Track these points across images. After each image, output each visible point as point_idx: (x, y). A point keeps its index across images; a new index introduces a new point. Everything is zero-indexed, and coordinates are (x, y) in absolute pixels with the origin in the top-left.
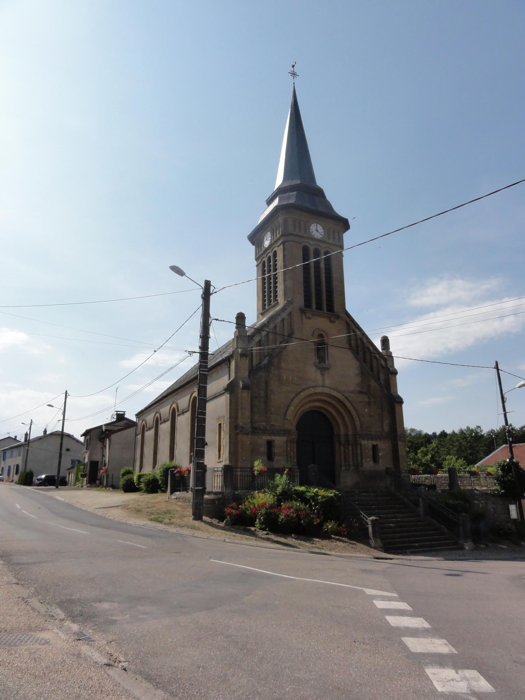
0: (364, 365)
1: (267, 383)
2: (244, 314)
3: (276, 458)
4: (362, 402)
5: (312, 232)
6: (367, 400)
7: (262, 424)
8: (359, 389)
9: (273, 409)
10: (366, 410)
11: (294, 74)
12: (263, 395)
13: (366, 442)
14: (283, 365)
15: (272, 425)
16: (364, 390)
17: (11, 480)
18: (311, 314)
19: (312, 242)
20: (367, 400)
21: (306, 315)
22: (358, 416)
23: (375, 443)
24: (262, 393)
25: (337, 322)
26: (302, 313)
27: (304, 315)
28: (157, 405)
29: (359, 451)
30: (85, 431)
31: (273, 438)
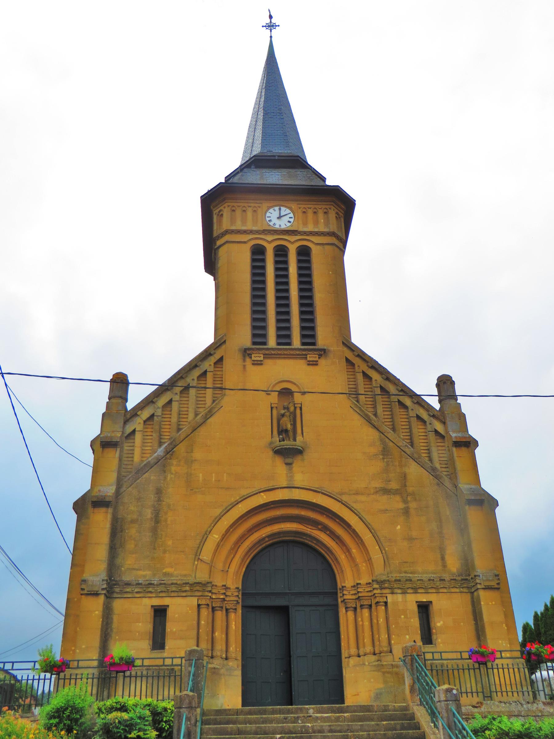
0: (391, 434)
1: (159, 492)
2: (126, 376)
3: (169, 643)
4: (385, 511)
5: (274, 224)
6: (401, 506)
7: (141, 573)
8: (377, 484)
9: (170, 543)
10: (399, 527)
11: (271, 26)
12: (149, 516)
13: (399, 598)
14: (198, 454)
15: (165, 574)
16: (394, 485)
17: (361, 663)
18: (262, 356)
19: (270, 238)
20: (401, 506)
21: (251, 357)
22: (378, 542)
23: (424, 598)
24: (148, 513)
25: (323, 362)
26: (244, 356)
27: (248, 360)
28: (215, 557)
29: (381, 620)
30: (550, 599)
31: (166, 601)
